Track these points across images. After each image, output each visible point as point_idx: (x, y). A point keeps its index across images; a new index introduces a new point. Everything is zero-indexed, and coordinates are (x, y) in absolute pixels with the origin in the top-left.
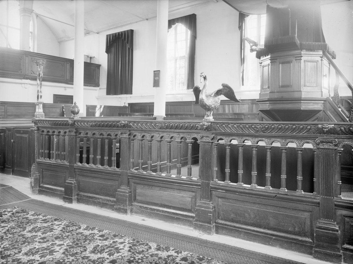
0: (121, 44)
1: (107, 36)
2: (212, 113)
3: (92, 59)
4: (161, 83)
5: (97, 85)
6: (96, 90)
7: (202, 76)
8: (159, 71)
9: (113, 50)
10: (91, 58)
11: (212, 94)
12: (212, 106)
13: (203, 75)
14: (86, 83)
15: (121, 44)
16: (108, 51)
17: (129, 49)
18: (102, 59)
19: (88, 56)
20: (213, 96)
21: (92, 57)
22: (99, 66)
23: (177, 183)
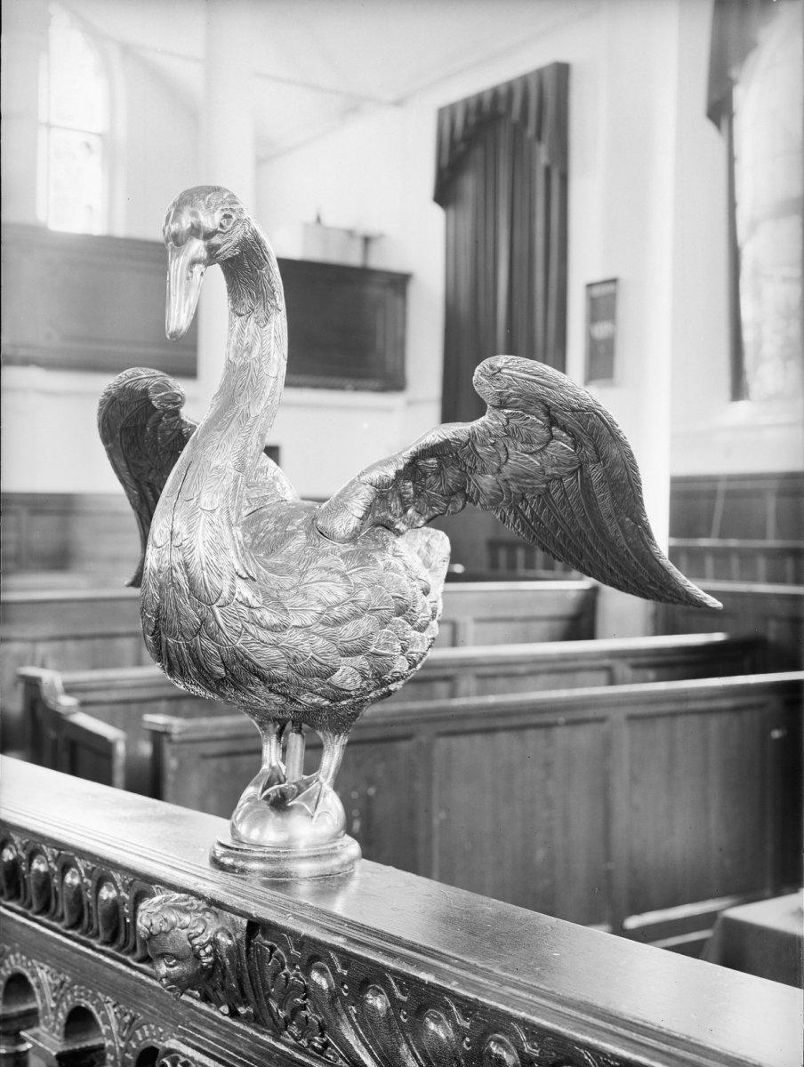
0: (502, 151)
1: (441, 112)
2: (331, 758)
3: (374, 248)
4: (624, 359)
5: (393, 381)
6: (389, 410)
7: (195, 231)
8: (614, 281)
9: (469, 185)
10: (367, 240)
11: (340, 505)
12: (336, 679)
13: (210, 221)
14: (294, 379)
15: (502, 151)
16: (445, 193)
17: (548, 171)
18: (417, 240)
19: (350, 233)
20: (353, 538)
21: (369, 234)
22: (399, 282)
23: (596, 1016)
